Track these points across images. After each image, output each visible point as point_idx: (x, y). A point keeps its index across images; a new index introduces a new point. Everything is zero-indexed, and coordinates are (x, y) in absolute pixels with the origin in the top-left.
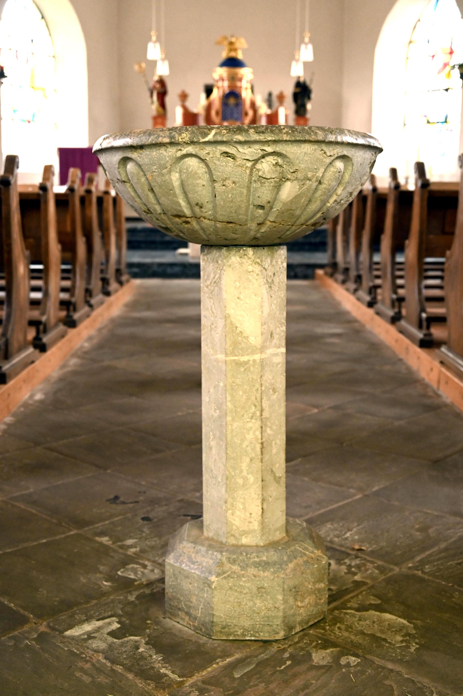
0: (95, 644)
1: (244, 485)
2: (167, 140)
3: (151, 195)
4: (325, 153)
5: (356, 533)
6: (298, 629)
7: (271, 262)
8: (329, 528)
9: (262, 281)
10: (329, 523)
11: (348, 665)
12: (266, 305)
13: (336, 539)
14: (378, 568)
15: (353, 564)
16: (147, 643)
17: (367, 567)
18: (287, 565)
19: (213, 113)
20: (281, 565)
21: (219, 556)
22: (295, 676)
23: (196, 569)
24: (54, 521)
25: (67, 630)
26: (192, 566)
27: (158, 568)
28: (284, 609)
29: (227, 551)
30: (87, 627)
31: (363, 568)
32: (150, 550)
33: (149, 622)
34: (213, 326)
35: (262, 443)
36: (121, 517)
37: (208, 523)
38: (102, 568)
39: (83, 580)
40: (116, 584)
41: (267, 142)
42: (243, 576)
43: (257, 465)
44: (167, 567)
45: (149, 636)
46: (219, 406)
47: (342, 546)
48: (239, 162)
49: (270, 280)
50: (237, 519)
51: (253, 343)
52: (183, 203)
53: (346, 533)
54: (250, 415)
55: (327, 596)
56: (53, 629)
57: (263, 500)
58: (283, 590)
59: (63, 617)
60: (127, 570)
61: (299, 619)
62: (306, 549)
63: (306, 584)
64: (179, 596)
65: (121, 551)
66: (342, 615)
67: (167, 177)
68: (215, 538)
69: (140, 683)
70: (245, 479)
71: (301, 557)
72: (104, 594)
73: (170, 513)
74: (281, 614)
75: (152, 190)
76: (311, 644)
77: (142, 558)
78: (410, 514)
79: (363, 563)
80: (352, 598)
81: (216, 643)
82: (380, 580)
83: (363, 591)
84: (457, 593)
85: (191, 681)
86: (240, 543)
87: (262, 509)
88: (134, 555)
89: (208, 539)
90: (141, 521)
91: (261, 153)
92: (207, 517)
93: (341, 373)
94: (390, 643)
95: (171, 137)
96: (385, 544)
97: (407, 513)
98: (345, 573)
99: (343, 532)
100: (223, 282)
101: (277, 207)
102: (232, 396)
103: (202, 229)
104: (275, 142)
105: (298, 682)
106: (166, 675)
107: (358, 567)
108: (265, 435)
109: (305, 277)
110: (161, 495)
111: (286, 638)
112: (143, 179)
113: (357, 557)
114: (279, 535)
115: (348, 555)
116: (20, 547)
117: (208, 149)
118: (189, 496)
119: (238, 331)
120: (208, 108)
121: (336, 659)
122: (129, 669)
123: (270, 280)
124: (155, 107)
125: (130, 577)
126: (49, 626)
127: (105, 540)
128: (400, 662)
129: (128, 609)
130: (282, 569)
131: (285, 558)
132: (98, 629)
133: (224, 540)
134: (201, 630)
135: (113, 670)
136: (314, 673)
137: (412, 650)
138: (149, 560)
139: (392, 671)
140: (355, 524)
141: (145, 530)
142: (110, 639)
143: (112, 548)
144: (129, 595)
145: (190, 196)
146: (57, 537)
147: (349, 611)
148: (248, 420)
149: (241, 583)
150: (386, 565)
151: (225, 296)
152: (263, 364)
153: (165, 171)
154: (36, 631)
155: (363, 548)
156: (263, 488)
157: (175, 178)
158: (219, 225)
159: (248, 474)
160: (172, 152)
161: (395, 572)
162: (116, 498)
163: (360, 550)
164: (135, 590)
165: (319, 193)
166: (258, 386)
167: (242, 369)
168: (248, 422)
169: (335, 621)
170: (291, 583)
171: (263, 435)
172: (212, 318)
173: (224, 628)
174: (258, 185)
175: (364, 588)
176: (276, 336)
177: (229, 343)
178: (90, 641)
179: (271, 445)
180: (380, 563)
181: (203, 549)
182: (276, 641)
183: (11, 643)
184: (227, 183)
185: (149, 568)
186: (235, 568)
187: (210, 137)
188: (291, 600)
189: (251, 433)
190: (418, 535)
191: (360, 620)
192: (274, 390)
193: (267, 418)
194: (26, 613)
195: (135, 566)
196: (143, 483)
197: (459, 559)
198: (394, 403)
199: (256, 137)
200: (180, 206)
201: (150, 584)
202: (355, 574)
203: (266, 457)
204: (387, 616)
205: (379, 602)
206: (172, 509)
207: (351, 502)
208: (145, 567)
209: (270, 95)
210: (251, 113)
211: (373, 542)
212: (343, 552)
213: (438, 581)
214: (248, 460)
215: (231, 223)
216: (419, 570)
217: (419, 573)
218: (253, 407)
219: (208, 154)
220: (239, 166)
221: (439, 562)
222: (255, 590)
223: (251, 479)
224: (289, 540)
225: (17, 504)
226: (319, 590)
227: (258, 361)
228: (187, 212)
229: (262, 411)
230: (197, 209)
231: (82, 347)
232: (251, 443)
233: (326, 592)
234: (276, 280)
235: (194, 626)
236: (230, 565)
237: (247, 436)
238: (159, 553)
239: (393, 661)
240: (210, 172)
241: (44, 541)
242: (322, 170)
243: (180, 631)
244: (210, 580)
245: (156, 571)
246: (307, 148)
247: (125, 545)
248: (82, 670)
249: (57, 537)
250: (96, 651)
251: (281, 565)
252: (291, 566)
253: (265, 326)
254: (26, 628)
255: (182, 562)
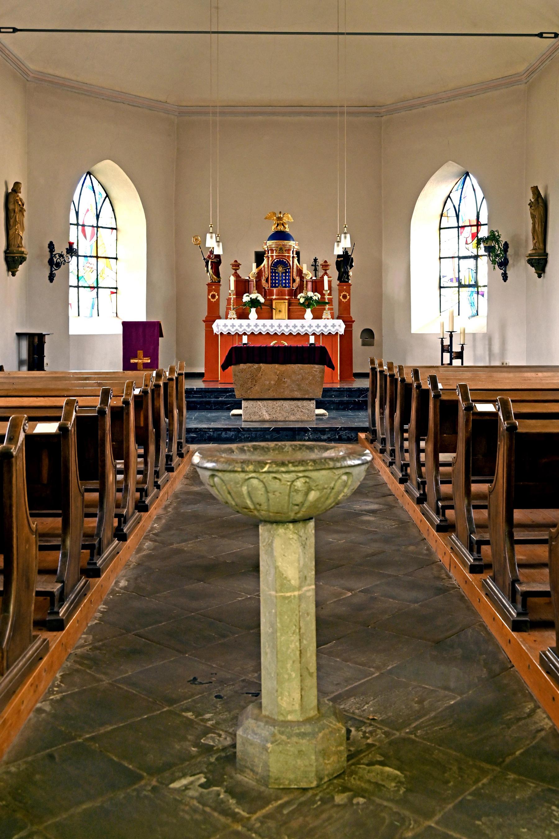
0: (191, 793)
1: (288, 679)
2: (239, 469)
3: (229, 496)
4: (335, 473)
5: (372, 706)
6: (326, 779)
7: (305, 531)
8: (353, 701)
9: (299, 544)
10: (353, 698)
11: (358, 804)
12: (302, 559)
13: (357, 711)
14: (385, 733)
15: (367, 730)
16: (225, 792)
17: (377, 732)
18: (318, 735)
19: (263, 281)
20: (314, 734)
21: (272, 729)
22: (322, 812)
23: (257, 739)
24: (150, 699)
25: (171, 783)
26: (255, 736)
27: (229, 736)
28: (316, 766)
29: (278, 725)
30: (185, 781)
31: (374, 734)
32: (223, 722)
33: (225, 777)
34: (268, 573)
35: (300, 651)
36: (200, 695)
37: (265, 705)
38: (189, 737)
39: (177, 747)
40: (201, 750)
41: (300, 472)
42: (289, 743)
43: (297, 665)
44: (238, 737)
45: (226, 786)
46: (272, 625)
47: (360, 716)
48: (283, 482)
49: (303, 543)
50: (284, 703)
51: (294, 584)
52: (249, 502)
53: (364, 705)
54: (293, 631)
55: (346, 756)
56: (162, 783)
57: (302, 689)
58: (315, 752)
59: (167, 774)
60: (208, 738)
61: (326, 772)
62: (331, 722)
63: (331, 747)
64: (246, 758)
65: (202, 723)
66: (357, 769)
67: (240, 489)
68: (270, 716)
69: (223, 819)
70: (290, 675)
71: (328, 728)
72: (193, 757)
73: (236, 692)
74: (314, 769)
75: (229, 493)
76: (334, 790)
77: (218, 729)
78: (413, 689)
79: (374, 730)
80: (364, 756)
81: (271, 791)
82: (385, 742)
83: (373, 751)
84: (437, 751)
85: (254, 817)
86: (287, 719)
87: (301, 695)
88: (211, 727)
89: (265, 716)
90: (215, 698)
91: (296, 477)
92: (265, 699)
93: (373, 555)
94: (387, 788)
95: (243, 468)
96: (391, 714)
97: (410, 688)
98: (361, 738)
99: (362, 706)
100: (274, 545)
101: (307, 504)
102: (281, 619)
103: (262, 516)
104: (304, 471)
105: (324, 816)
106: (238, 813)
107: (371, 733)
108: (302, 645)
109: (349, 440)
110: (229, 676)
111: (318, 786)
112: (224, 488)
113: (370, 725)
114: (313, 713)
115: (365, 723)
116: (129, 722)
117: (264, 475)
118: (251, 677)
119: (284, 577)
120: (259, 275)
121: (351, 799)
122: (215, 809)
123: (303, 543)
124: (209, 276)
125: (210, 743)
126: (157, 781)
127: (189, 715)
128: (392, 800)
129: (210, 767)
130: (315, 737)
131: (317, 730)
132: (192, 783)
133: (276, 718)
134: (261, 782)
135: (204, 811)
136: (335, 809)
137: (401, 792)
138: (222, 730)
139: (386, 807)
140: (372, 698)
141: (218, 706)
142: (201, 790)
143: (195, 721)
144: (210, 757)
145: (254, 499)
146: (155, 713)
147: (362, 766)
148: (291, 635)
149: (288, 748)
150: (390, 730)
151: (275, 554)
152: (300, 597)
153: (238, 486)
154: (150, 785)
155: (375, 718)
156: (302, 681)
157: (244, 489)
158: (271, 514)
159: (291, 671)
160: (243, 475)
161: (396, 736)
162: (195, 679)
163: (373, 719)
164: (215, 753)
165: (332, 495)
166: (297, 612)
167: (287, 602)
168: (291, 636)
169: (352, 773)
170: (320, 747)
171: (301, 645)
172: (267, 568)
173: (276, 779)
174: (294, 494)
175: (373, 749)
176: (308, 579)
177: (278, 584)
178: (187, 791)
179: (306, 651)
180: (386, 729)
181: (262, 724)
182: (312, 788)
183: (135, 794)
184: (276, 493)
185: (223, 736)
186: (284, 737)
187: (265, 469)
188: (321, 759)
189: (293, 643)
190: (416, 706)
191: (369, 772)
192: (308, 614)
193: (303, 633)
194: (141, 772)
195: (213, 735)
196: (214, 666)
197: (442, 725)
198: (413, 586)
199: (293, 469)
200: (247, 503)
201: (224, 749)
202: (368, 738)
203: (303, 660)
204: (387, 769)
205: (382, 759)
206: (237, 688)
207: (370, 680)
208: (220, 736)
209: (315, 260)
210: (298, 279)
211: (383, 713)
212: (361, 721)
213: (425, 742)
214: (291, 662)
215: (279, 513)
216: (412, 734)
217: (413, 737)
218: (294, 627)
219: (265, 478)
220: (283, 484)
221: (428, 728)
222: (296, 752)
223: (294, 675)
224: (319, 717)
225: (121, 686)
226: (340, 752)
227: (297, 596)
228: (252, 507)
229: (300, 629)
230: (258, 507)
231: (153, 528)
232: (293, 650)
233: (345, 753)
234: (308, 543)
235: (256, 779)
236: (280, 736)
237: (290, 646)
238: (230, 725)
239: (388, 800)
240: (265, 487)
241: (146, 716)
242: (333, 483)
243: (247, 783)
244: (267, 747)
245: (228, 739)
246: (324, 472)
247: (204, 719)
248: (183, 811)
249: (155, 713)
250: (192, 798)
251: (313, 735)
252: (321, 735)
253: (301, 573)
254: (143, 783)
255: (248, 734)
